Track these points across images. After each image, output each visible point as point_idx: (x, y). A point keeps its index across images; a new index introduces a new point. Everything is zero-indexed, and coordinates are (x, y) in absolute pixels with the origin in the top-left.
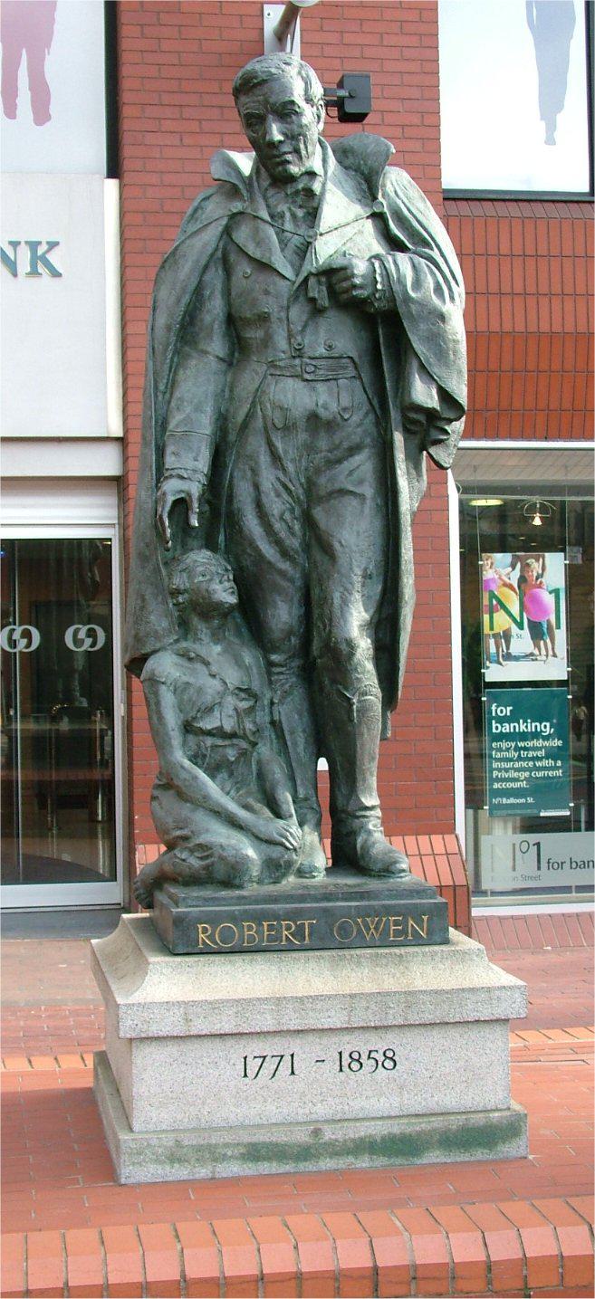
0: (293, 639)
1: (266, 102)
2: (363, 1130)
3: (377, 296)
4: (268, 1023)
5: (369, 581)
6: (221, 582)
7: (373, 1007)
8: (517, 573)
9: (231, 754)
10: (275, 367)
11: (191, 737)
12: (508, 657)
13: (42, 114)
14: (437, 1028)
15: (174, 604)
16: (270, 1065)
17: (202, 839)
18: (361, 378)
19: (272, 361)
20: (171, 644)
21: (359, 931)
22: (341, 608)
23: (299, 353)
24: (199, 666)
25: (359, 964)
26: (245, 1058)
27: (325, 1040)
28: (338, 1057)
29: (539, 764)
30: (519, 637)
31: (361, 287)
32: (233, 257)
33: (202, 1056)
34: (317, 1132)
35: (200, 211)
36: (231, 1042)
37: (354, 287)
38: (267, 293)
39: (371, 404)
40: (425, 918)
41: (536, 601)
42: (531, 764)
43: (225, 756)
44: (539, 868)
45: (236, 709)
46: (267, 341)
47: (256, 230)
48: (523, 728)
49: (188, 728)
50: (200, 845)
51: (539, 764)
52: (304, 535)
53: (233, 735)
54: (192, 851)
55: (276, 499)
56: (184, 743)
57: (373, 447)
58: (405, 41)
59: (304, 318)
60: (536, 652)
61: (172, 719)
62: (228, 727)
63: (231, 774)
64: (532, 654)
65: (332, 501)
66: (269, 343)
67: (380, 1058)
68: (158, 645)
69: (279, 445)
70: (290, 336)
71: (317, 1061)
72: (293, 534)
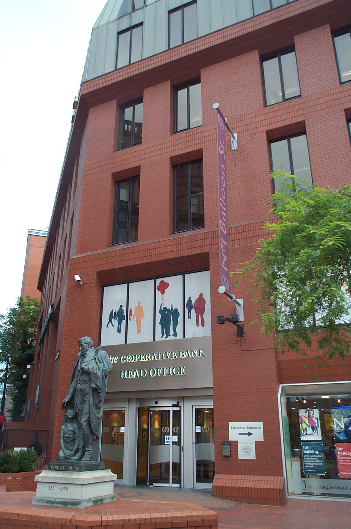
2: (60, 500)
8: (307, 414)
12: (306, 434)
13: (203, 325)
29: (316, 461)
30: (309, 429)
34: (55, 500)
41: (313, 421)
42: (314, 461)
44: (305, 487)
48: (311, 452)
49: (64, 437)
51: (316, 461)
53: (68, 438)
60: (313, 433)
61: (62, 435)
64: (312, 434)
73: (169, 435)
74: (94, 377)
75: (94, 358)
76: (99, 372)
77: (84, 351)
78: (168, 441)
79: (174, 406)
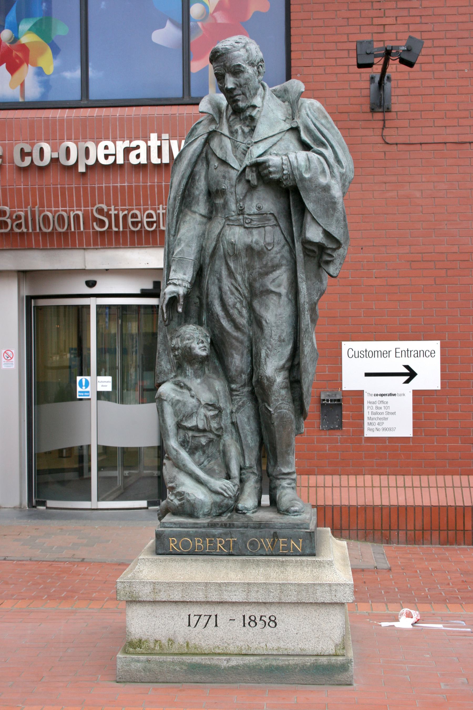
0: (243, 376)
1: (225, 65)
3: (284, 177)
4: (200, 597)
5: (283, 343)
6: (198, 344)
7: (261, 591)
9: (203, 441)
10: (229, 220)
11: (181, 431)
14: (301, 605)
15: (173, 356)
16: (203, 620)
17: (180, 489)
18: (279, 226)
19: (228, 217)
20: (172, 378)
21: (262, 546)
22: (265, 359)
23: (241, 212)
24: (185, 391)
25: (258, 565)
26: (189, 615)
27: (235, 608)
28: (243, 618)
31: (274, 173)
32: (210, 156)
33: (164, 613)
35: (195, 131)
36: (181, 606)
37: (270, 173)
38: (224, 177)
39: (286, 240)
40: (301, 540)
43: (200, 442)
45: (205, 416)
46: (225, 205)
47: (221, 141)
49: (179, 426)
50: (178, 492)
52: (250, 316)
53: (204, 431)
54: (176, 495)
55: (231, 296)
56: (177, 434)
57: (287, 266)
58: (407, 20)
59: (244, 191)
61: (170, 422)
62: (201, 426)
63: (204, 452)
65: (263, 297)
66: (226, 207)
67: (267, 621)
68: (165, 379)
69: (232, 265)
70: (237, 202)
71: (230, 620)
72: (242, 316)
73: (89, 374)
74: (317, 201)
75: (288, 126)
76: (333, 182)
77: (244, 94)
78: (84, 389)
79: (144, 294)
